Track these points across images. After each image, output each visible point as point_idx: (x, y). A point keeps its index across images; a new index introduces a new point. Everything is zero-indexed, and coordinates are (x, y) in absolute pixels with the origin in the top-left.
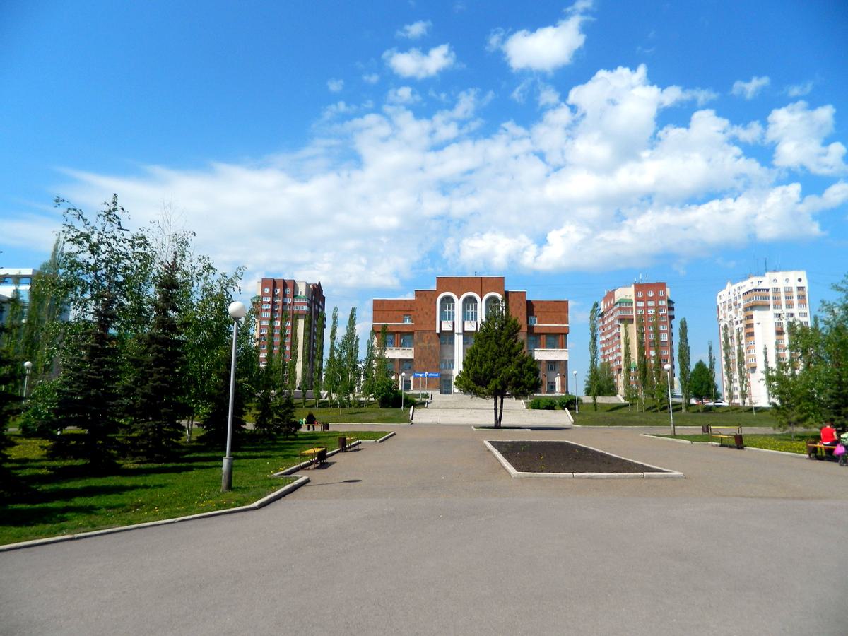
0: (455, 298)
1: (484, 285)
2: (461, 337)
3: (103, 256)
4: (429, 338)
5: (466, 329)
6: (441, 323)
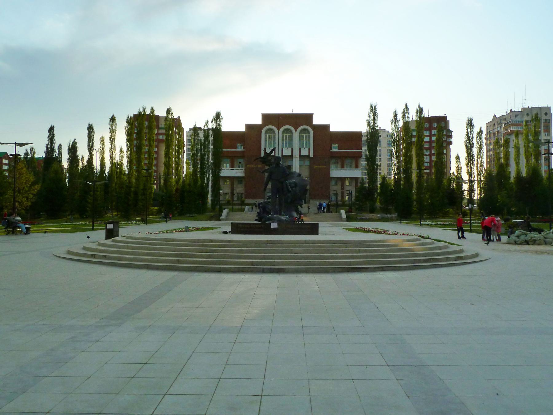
0: (292, 129)
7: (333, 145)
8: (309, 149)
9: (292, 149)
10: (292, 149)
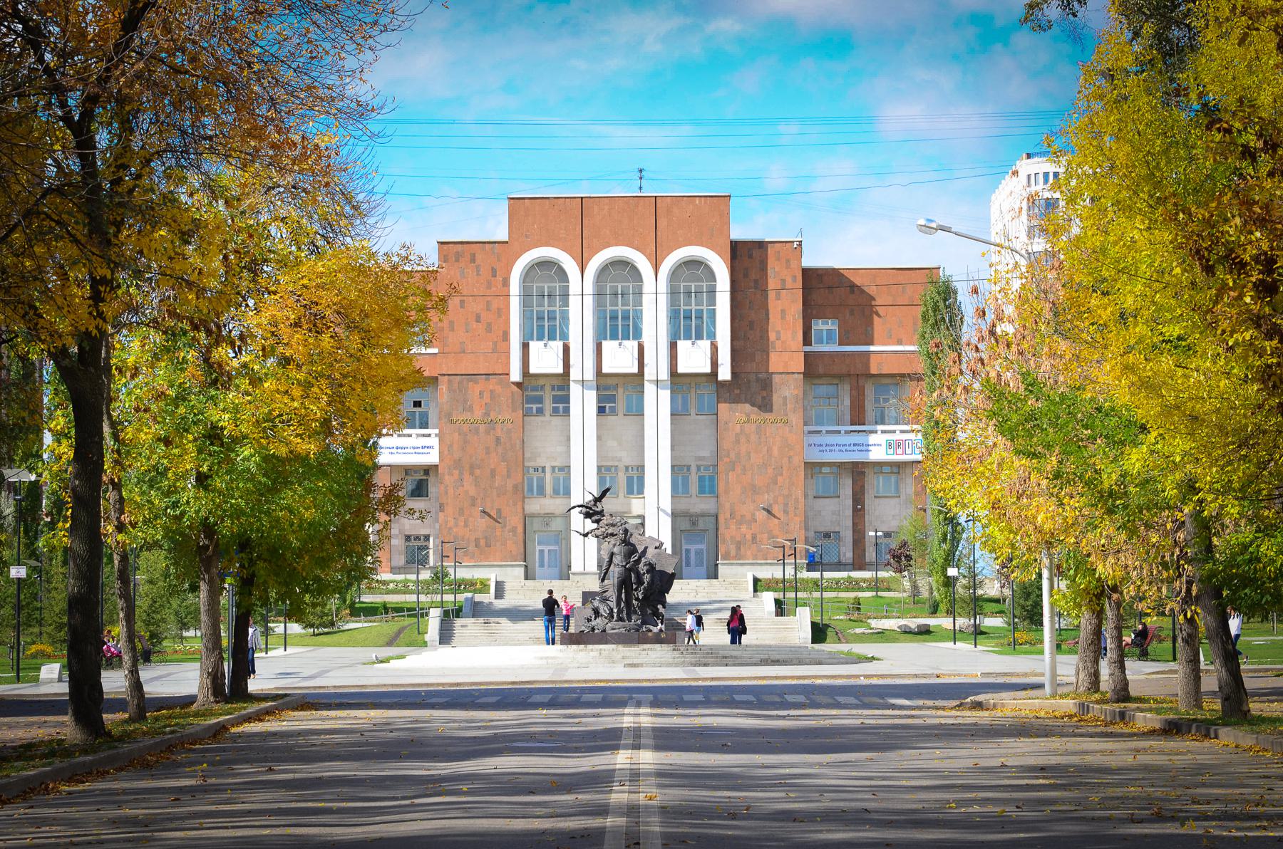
0: (643, 263)
1: (662, 223)
2: (666, 395)
3: (214, 415)
4: (487, 399)
5: (681, 369)
6: (525, 347)
7: (814, 327)
8: (714, 348)
9: (566, 350)
10: (566, 350)
